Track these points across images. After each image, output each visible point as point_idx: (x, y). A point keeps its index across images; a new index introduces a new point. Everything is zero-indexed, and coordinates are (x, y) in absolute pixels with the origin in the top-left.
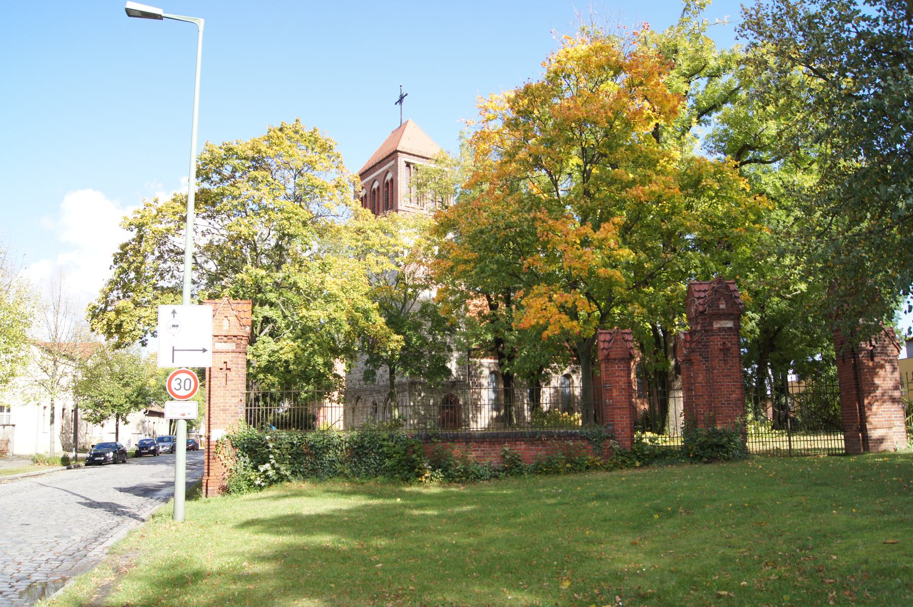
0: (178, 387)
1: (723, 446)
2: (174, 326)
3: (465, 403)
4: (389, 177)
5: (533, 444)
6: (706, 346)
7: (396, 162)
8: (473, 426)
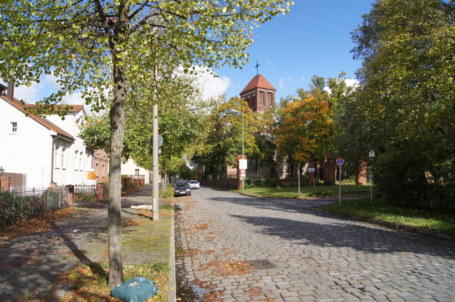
3: (278, 170)
4: (254, 95)
7: (257, 91)
8: (281, 178)
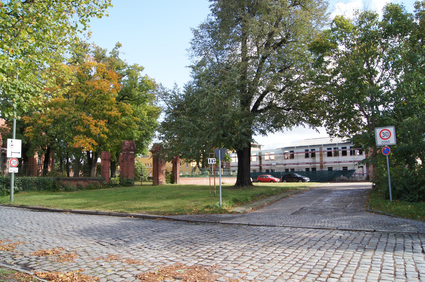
0: (384, 136)
1: (130, 183)
2: (12, 145)
5: (85, 181)
6: (127, 158)
